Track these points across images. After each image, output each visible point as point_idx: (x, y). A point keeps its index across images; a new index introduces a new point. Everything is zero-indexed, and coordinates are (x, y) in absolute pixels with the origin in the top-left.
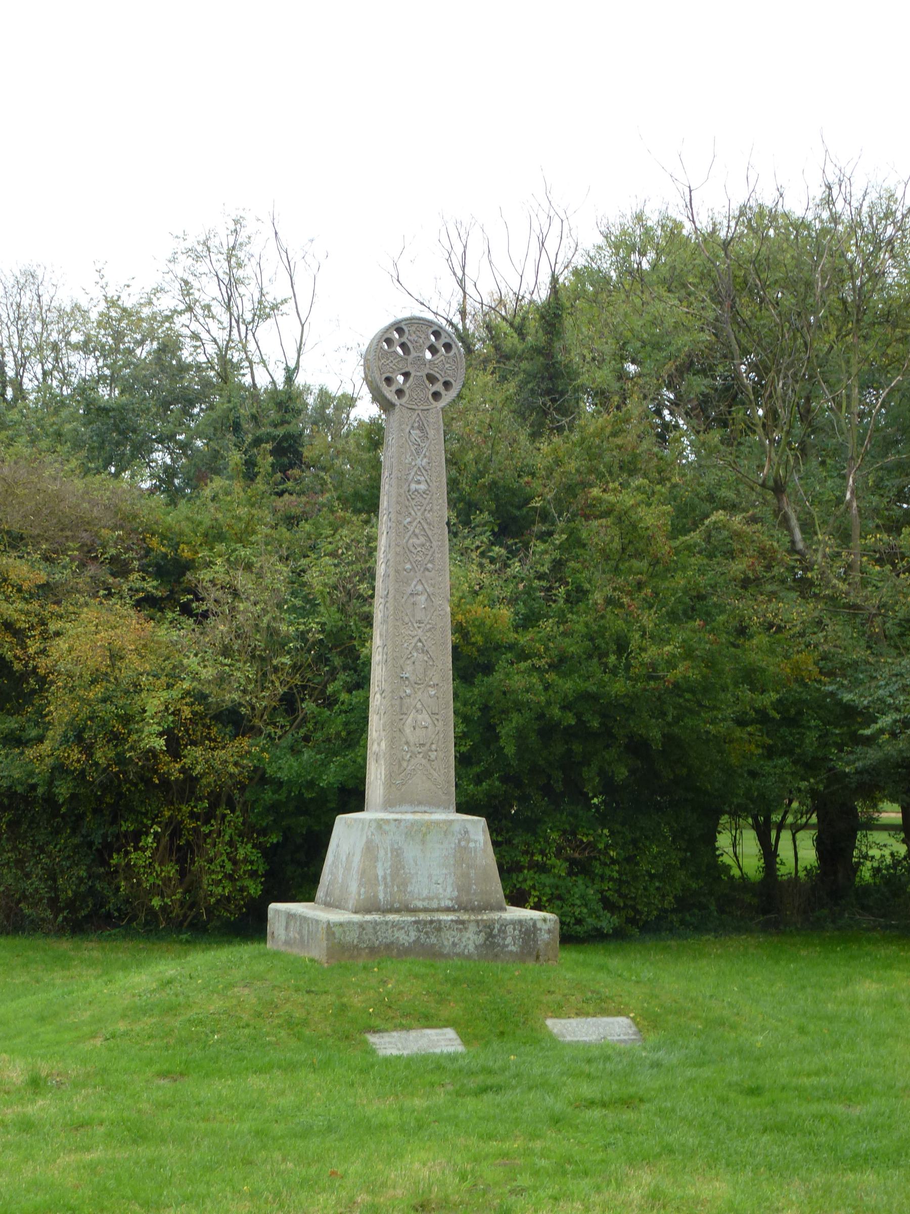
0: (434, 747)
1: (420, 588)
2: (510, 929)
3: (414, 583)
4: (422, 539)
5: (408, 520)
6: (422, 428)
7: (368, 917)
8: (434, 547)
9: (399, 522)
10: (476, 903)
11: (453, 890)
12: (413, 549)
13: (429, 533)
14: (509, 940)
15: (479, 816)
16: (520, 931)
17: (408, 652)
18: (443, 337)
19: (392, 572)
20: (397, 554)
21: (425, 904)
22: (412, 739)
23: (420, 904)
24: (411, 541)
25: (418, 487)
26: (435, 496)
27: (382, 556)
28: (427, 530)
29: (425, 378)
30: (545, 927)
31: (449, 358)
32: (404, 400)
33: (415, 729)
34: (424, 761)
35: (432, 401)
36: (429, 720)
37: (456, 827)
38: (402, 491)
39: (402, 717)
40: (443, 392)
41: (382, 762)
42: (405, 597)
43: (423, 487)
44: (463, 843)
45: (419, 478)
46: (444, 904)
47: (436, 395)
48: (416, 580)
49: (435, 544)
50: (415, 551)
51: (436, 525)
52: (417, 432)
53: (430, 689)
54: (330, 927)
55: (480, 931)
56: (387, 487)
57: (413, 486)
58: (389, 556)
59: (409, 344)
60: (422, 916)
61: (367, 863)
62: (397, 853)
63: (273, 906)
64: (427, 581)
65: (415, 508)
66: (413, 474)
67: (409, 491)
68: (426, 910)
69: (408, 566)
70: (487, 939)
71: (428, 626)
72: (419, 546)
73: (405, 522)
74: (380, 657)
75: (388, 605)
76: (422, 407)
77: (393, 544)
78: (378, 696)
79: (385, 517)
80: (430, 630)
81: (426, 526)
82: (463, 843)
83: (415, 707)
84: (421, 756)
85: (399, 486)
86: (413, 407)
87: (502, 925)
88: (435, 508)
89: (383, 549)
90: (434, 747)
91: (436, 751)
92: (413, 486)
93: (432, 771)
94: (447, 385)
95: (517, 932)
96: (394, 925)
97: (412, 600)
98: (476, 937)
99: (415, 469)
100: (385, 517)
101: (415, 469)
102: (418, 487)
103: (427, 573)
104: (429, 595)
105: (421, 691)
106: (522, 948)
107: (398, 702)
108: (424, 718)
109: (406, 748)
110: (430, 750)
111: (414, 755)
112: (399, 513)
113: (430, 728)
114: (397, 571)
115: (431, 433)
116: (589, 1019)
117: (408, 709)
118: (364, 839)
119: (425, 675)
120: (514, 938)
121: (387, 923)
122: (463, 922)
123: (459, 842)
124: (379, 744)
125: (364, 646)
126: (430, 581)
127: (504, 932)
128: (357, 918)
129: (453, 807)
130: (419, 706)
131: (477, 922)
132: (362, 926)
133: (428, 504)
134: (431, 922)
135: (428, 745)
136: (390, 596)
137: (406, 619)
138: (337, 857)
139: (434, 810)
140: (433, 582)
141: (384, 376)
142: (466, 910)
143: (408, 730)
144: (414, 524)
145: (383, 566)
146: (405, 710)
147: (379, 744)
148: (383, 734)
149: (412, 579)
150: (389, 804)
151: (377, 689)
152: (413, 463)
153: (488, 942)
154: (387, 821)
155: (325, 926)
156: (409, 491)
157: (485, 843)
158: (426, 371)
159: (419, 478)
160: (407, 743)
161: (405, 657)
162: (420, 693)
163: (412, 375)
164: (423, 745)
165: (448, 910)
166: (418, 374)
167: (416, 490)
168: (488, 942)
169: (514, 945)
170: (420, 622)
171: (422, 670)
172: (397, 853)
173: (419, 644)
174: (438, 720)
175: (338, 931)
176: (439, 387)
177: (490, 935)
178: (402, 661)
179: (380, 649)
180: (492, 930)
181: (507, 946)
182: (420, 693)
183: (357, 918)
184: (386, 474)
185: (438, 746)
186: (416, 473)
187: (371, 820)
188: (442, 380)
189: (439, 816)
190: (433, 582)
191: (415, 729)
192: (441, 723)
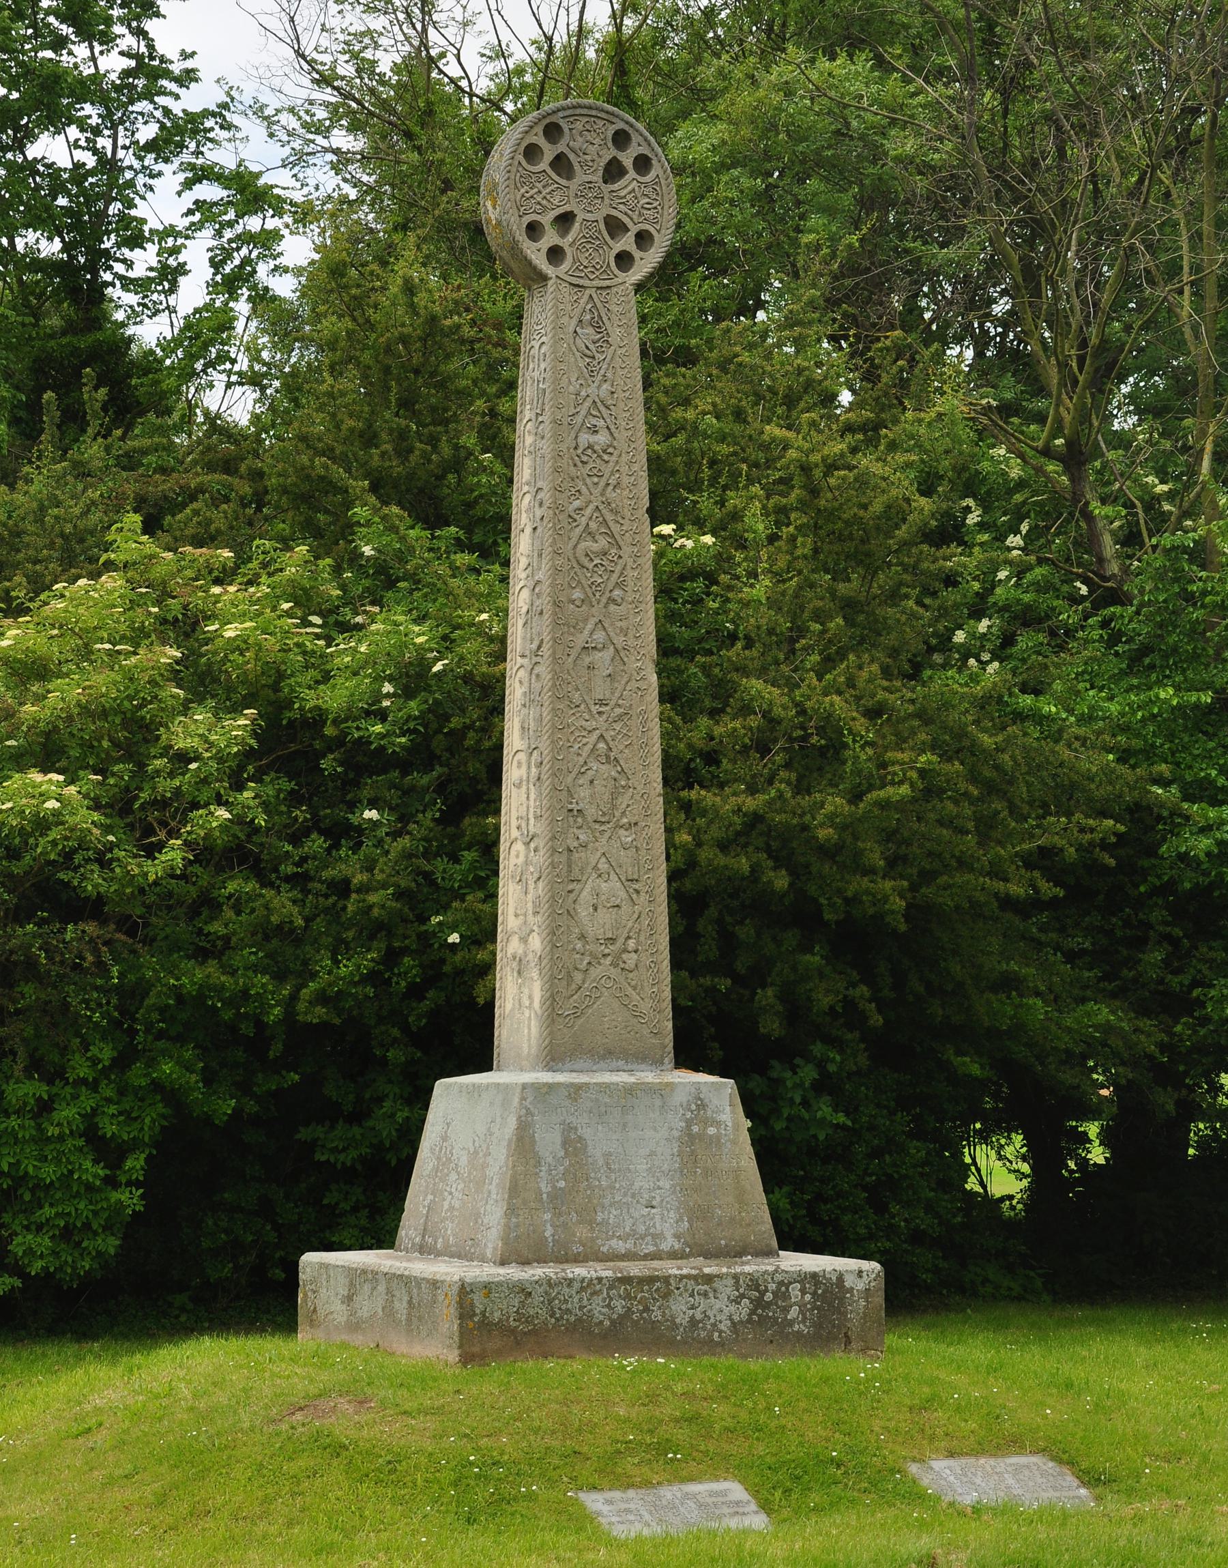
0: (631, 944)
1: (600, 636)
2: (795, 1291)
3: (590, 626)
4: (603, 542)
5: (577, 504)
6: (598, 326)
7: (537, 1272)
8: (625, 556)
9: (557, 508)
10: (723, 1242)
11: (680, 1220)
12: (585, 561)
13: (615, 528)
14: (793, 1313)
15: (711, 1073)
16: (814, 1294)
17: (581, 760)
18: (634, 144)
19: (545, 602)
20: (556, 571)
21: (629, 1245)
22: (593, 931)
23: (620, 1246)
24: (583, 545)
25: (593, 439)
26: (625, 458)
27: (523, 575)
28: (611, 524)
29: (602, 226)
30: (861, 1285)
31: (646, 185)
32: (565, 266)
33: (596, 909)
34: (614, 972)
35: (616, 271)
36: (623, 894)
37: (680, 1097)
38: (564, 447)
39: (570, 887)
40: (637, 254)
41: (535, 974)
42: (574, 653)
43: (602, 438)
44: (695, 1129)
45: (594, 421)
46: (665, 1246)
47: (624, 260)
48: (593, 621)
49: (627, 551)
50: (591, 566)
51: (627, 514)
52: (590, 330)
53: (622, 832)
54: (465, 1290)
55: (742, 1296)
56: (529, 440)
57: (585, 438)
58: (540, 576)
59: (572, 156)
60: (635, 1269)
61: (520, 1168)
62: (573, 1145)
63: (310, 1259)
64: (612, 624)
65: (588, 481)
66: (583, 412)
67: (576, 448)
68: (629, 1256)
69: (577, 594)
70: (753, 1312)
71: (618, 711)
72: (597, 554)
73: (571, 508)
74: (523, 771)
75: (537, 670)
76: (597, 283)
77: (548, 550)
78: (519, 847)
79: (528, 498)
80: (620, 718)
81: (609, 517)
82: (695, 1129)
83: (595, 868)
84: (608, 961)
85: (557, 438)
86: (581, 282)
87: (781, 1283)
88: (626, 480)
89: (524, 562)
90: (631, 944)
91: (636, 952)
92: (585, 438)
93: (630, 991)
94: (643, 239)
95: (808, 1297)
96: (587, 1286)
97: (587, 660)
98: (733, 1308)
99: (587, 404)
100: (528, 498)
101: (587, 404)
102: (593, 439)
103: (612, 607)
104: (617, 650)
105: (607, 835)
106: (818, 1326)
107: (563, 858)
108: (613, 887)
109: (579, 946)
110: (626, 951)
111: (595, 961)
112: (557, 489)
113: (624, 908)
114: (557, 604)
115: (616, 334)
116: (982, 1461)
117: (582, 870)
118: (512, 1123)
119: (614, 807)
120: (802, 1306)
121: (570, 1282)
122: (709, 1279)
123: (689, 1127)
124: (524, 940)
125: (991, 697)
126: (619, 624)
127: (786, 1296)
128: (514, 1273)
129: (669, 1059)
130: (603, 866)
131: (736, 1277)
132: (523, 1290)
133: (612, 474)
134: (651, 1280)
135: (622, 940)
136: (545, 648)
137: (576, 697)
138: (445, 1162)
139: (635, 1066)
140: (623, 624)
141: (526, 220)
142: (707, 1255)
143: (583, 912)
144: (588, 511)
145: (525, 594)
146: (576, 873)
147: (524, 940)
148: (531, 919)
149: (586, 620)
150: (553, 1057)
151: (515, 833)
152: (583, 393)
153: (755, 1318)
154: (551, 1087)
155: (455, 1289)
156: (576, 448)
157: (736, 1127)
158: (607, 211)
159: (594, 421)
160: (582, 937)
161: (576, 771)
162: (604, 840)
163: (579, 219)
164: (612, 940)
165: (674, 1255)
166: (589, 216)
167: (590, 447)
168: (755, 1318)
169: (804, 1321)
170: (601, 702)
171: (607, 797)
172: (573, 1145)
173: (602, 745)
174: (637, 892)
175: (478, 1300)
176: (626, 242)
177: (758, 1303)
178: (569, 779)
179: (522, 756)
180: (763, 1294)
181: (791, 1323)
182: (604, 840)
183: (514, 1273)
184: (528, 414)
185: (638, 943)
186: (589, 413)
187: (524, 1086)
188: (634, 230)
189: (649, 1076)
190: (623, 624)
191: (596, 909)
192: (643, 898)
